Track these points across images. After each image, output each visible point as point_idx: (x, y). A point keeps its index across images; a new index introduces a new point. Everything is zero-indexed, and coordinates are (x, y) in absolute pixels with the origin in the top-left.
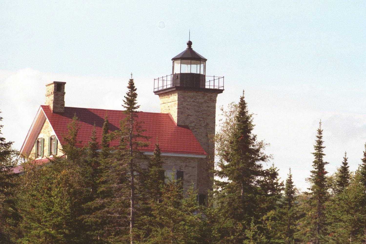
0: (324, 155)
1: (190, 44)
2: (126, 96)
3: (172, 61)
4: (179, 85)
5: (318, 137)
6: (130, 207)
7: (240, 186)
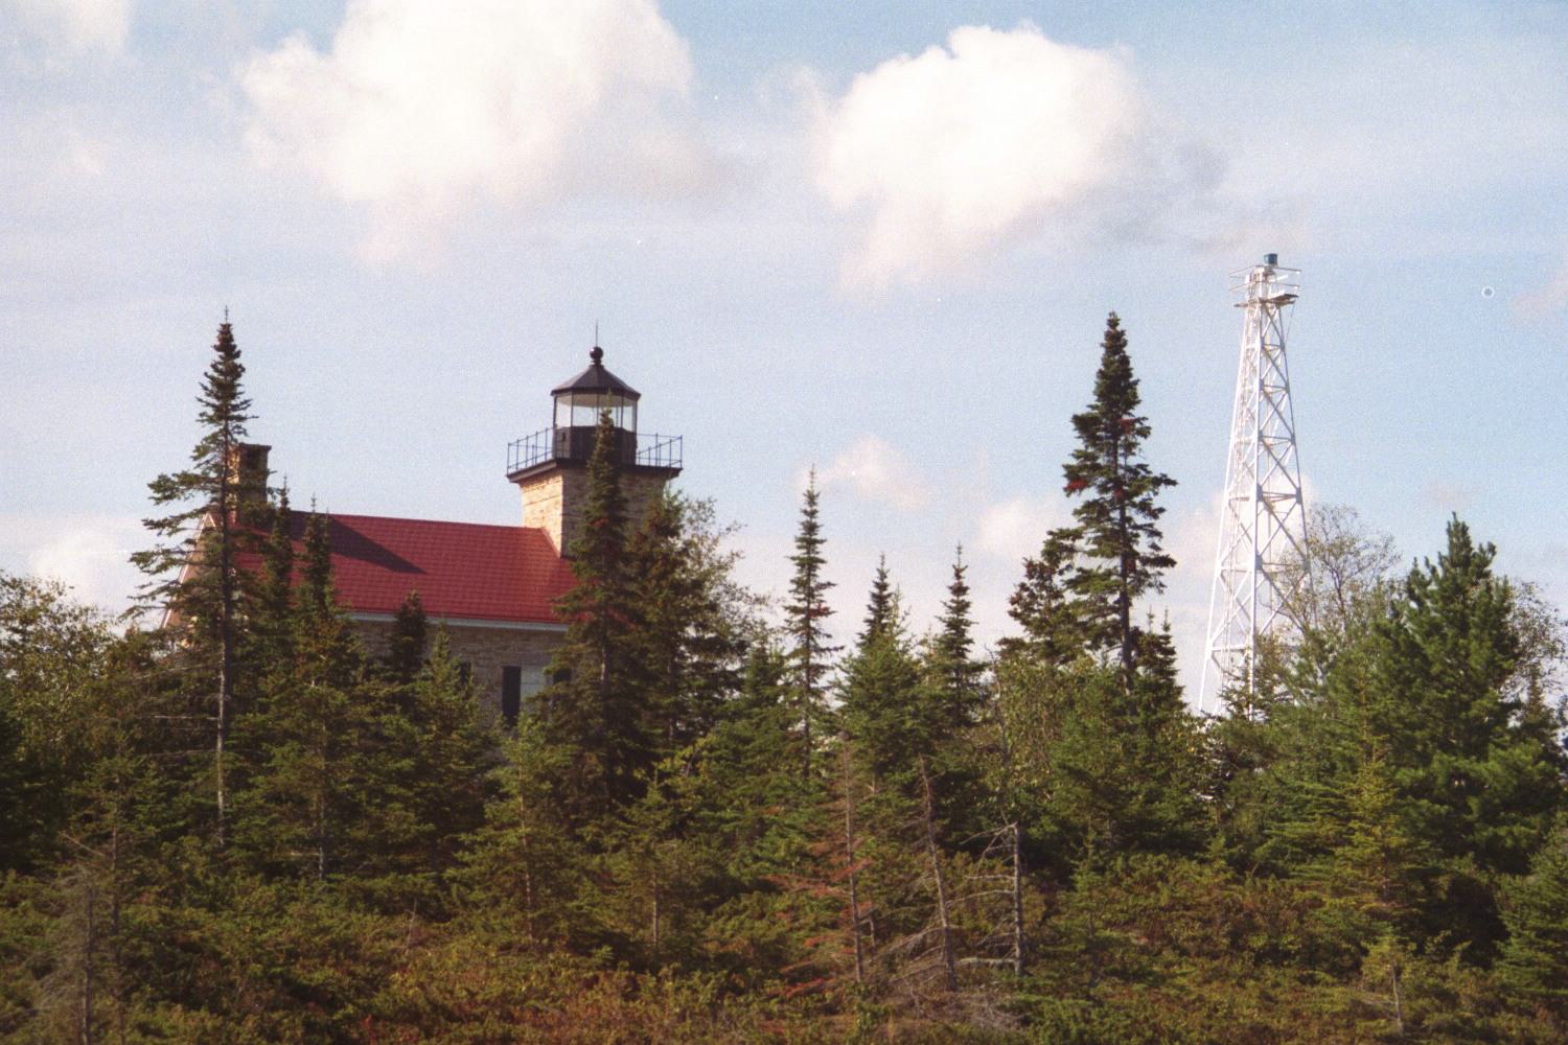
0: (822, 562)
1: (597, 354)
2: (211, 372)
3: (552, 399)
4: (567, 455)
5: (805, 512)
6: (218, 691)
7: (600, 653)
